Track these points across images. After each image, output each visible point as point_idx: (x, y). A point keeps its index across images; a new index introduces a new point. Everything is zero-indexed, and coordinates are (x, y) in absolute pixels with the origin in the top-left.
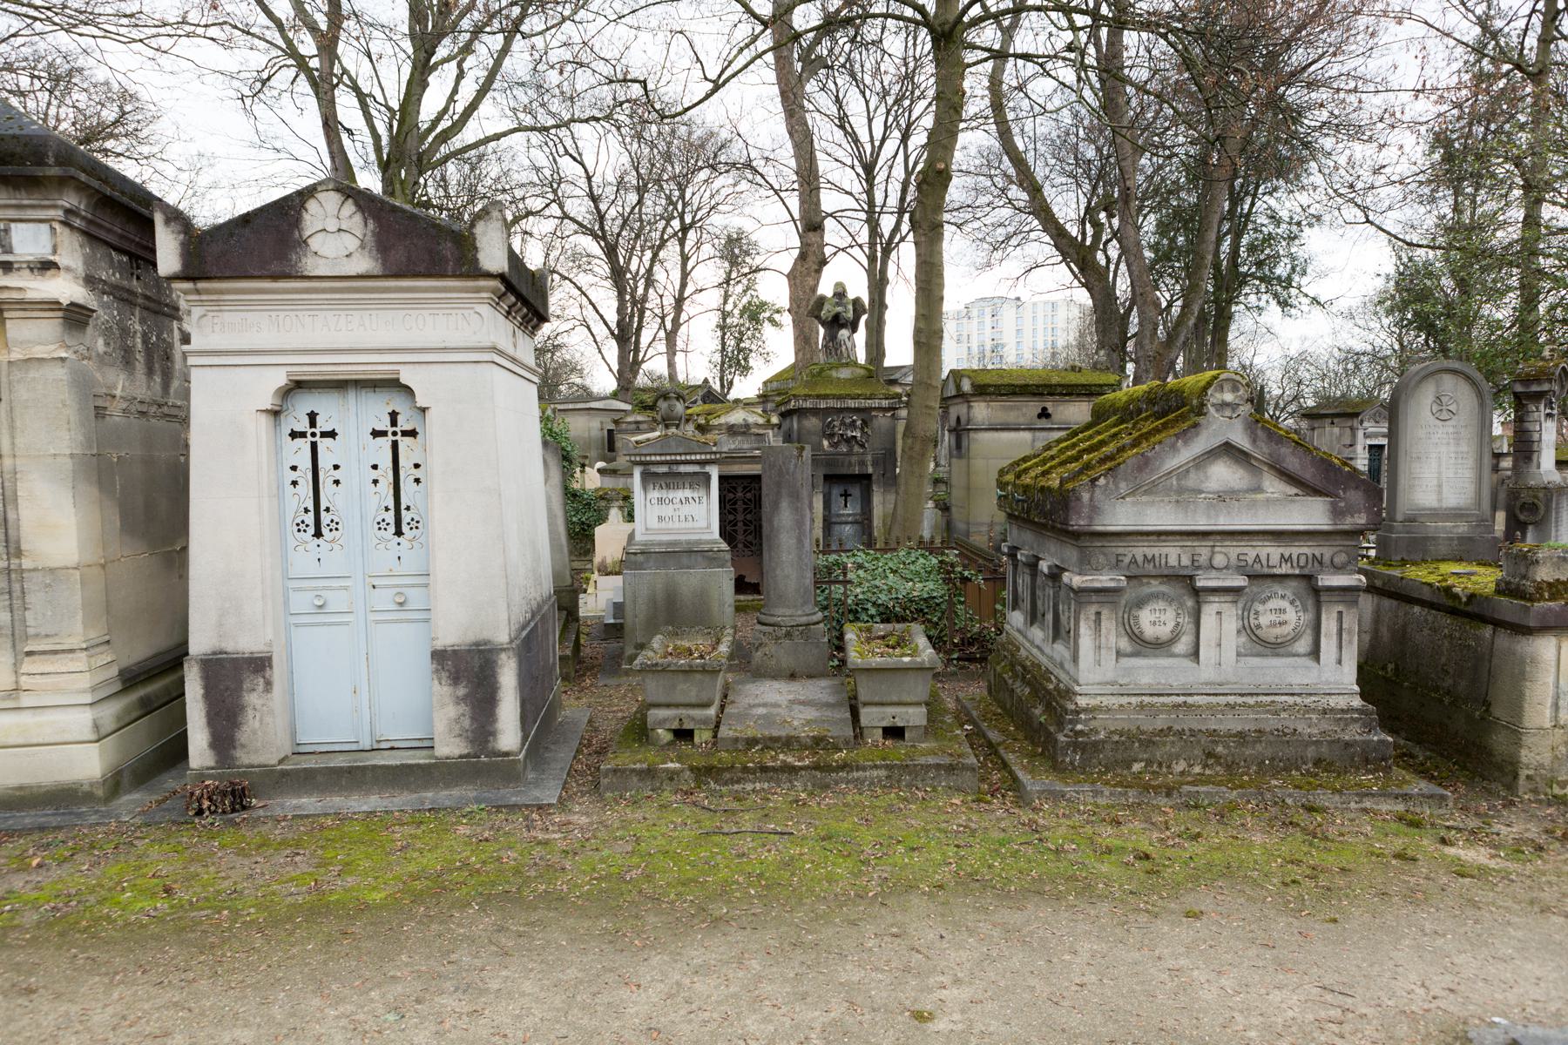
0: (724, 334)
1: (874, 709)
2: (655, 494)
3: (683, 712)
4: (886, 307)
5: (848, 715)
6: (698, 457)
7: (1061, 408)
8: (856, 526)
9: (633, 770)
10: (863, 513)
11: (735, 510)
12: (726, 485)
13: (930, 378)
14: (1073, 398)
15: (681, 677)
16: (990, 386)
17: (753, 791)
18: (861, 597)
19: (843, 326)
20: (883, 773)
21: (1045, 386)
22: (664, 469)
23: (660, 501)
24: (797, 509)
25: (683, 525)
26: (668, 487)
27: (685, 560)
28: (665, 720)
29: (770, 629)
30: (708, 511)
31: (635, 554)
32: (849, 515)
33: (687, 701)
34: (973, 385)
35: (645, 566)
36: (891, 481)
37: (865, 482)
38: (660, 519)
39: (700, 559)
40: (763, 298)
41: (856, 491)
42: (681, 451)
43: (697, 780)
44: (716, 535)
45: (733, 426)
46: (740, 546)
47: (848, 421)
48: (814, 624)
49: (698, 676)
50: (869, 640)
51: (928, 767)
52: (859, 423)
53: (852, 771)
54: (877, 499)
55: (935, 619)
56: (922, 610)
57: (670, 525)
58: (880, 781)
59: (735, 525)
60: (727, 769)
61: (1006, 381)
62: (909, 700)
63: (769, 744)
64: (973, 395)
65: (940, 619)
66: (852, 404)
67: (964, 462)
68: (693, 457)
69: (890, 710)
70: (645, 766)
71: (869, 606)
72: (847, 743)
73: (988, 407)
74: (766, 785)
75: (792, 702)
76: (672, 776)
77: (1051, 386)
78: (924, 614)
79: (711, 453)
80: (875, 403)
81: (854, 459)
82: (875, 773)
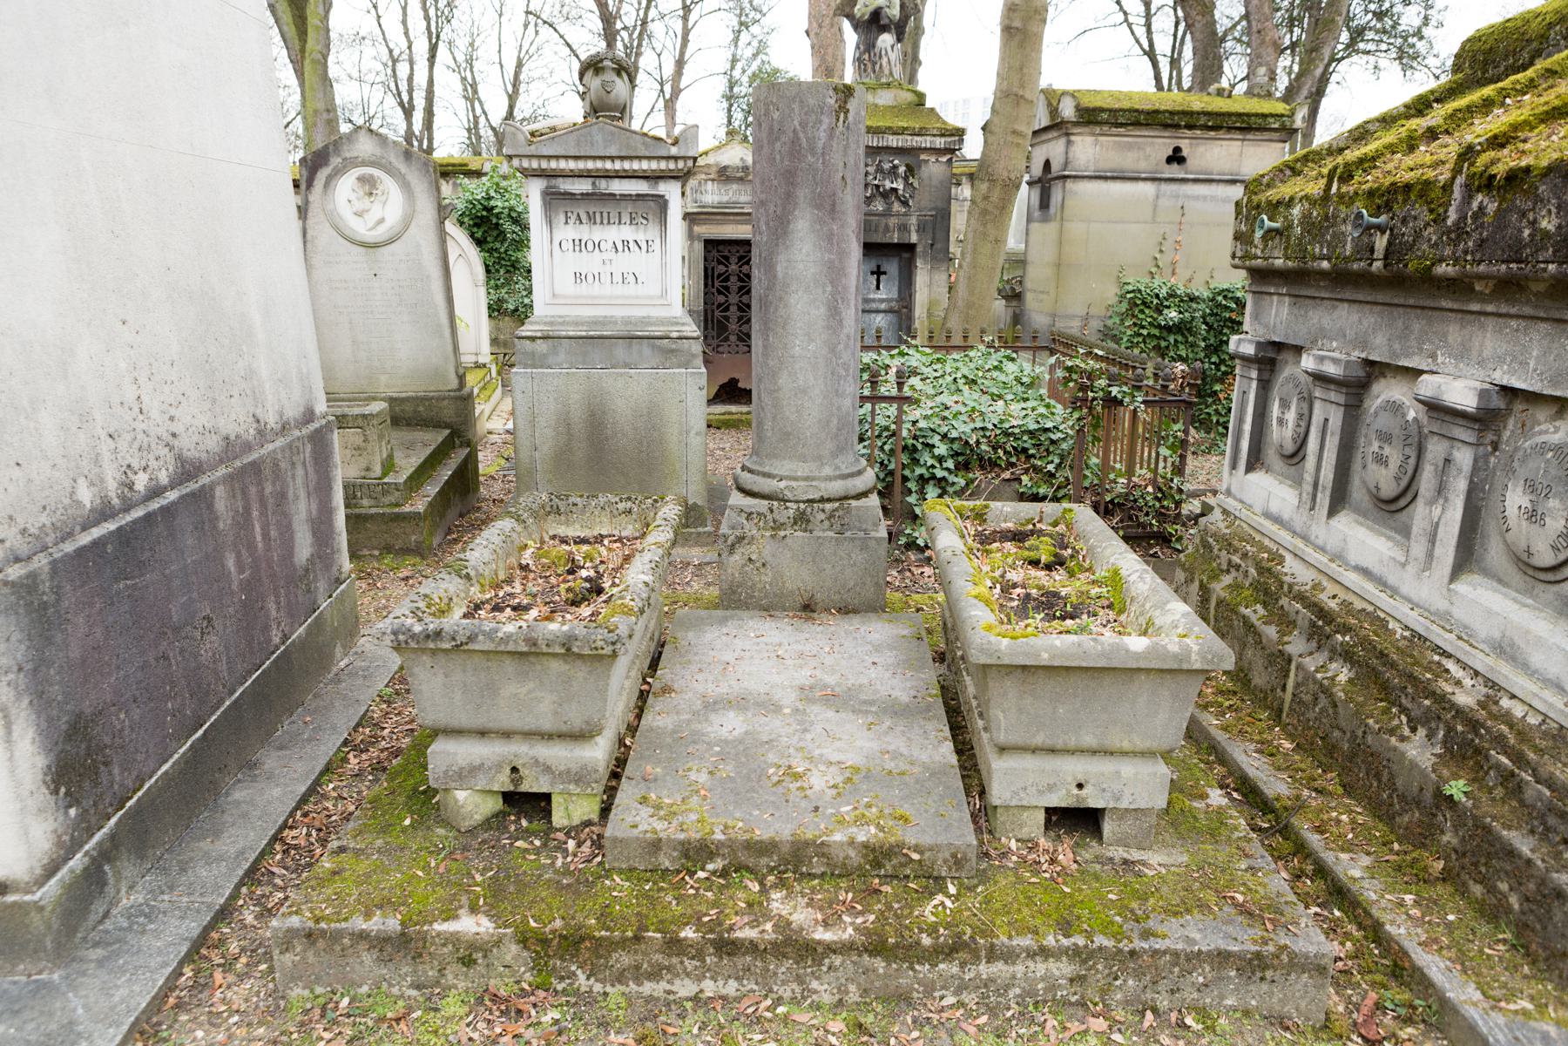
0: (731, 105)
1: (1029, 762)
2: (568, 232)
3: (521, 751)
4: (920, 64)
5: (948, 749)
6: (645, 165)
7: (1201, 149)
8: (890, 317)
9: (362, 936)
10: (901, 298)
11: (727, 288)
12: (714, 253)
13: (1022, 86)
14: (1221, 134)
15: (509, 665)
16: (1102, 110)
17: (695, 999)
18: (922, 424)
19: (884, 29)
20: (1063, 969)
21: (1184, 113)
22: (583, 186)
23: (579, 245)
24: (830, 237)
25: (619, 290)
26: (591, 219)
27: (620, 350)
28: (474, 770)
29: (762, 505)
30: (664, 265)
31: (533, 339)
32: (882, 301)
33: (530, 723)
34: (1078, 108)
35: (551, 360)
36: (941, 255)
37: (906, 255)
38: (578, 277)
40: (776, 63)
41: (892, 267)
42: (613, 151)
43: (538, 966)
44: (677, 310)
45: (725, 168)
46: (733, 338)
47: (887, 166)
48: (858, 496)
49: (556, 666)
50: (984, 539)
51: (1194, 959)
52: (902, 169)
53: (976, 958)
54: (922, 277)
55: (1051, 467)
56: (1025, 450)
57: (596, 289)
58: (1052, 988)
59: (727, 309)
60: (623, 944)
61: (1126, 105)
62: (1126, 745)
63: (743, 857)
64: (1076, 124)
65: (1058, 467)
66: (893, 141)
67: (1051, 228)
68: (636, 165)
69: (1074, 768)
70: (393, 924)
71: (936, 440)
72: (958, 862)
74: (731, 988)
75: (809, 694)
76: (469, 954)
77: (1191, 114)
78: (1029, 457)
79: (668, 158)
80: (926, 142)
81: (893, 221)
82: (1040, 968)
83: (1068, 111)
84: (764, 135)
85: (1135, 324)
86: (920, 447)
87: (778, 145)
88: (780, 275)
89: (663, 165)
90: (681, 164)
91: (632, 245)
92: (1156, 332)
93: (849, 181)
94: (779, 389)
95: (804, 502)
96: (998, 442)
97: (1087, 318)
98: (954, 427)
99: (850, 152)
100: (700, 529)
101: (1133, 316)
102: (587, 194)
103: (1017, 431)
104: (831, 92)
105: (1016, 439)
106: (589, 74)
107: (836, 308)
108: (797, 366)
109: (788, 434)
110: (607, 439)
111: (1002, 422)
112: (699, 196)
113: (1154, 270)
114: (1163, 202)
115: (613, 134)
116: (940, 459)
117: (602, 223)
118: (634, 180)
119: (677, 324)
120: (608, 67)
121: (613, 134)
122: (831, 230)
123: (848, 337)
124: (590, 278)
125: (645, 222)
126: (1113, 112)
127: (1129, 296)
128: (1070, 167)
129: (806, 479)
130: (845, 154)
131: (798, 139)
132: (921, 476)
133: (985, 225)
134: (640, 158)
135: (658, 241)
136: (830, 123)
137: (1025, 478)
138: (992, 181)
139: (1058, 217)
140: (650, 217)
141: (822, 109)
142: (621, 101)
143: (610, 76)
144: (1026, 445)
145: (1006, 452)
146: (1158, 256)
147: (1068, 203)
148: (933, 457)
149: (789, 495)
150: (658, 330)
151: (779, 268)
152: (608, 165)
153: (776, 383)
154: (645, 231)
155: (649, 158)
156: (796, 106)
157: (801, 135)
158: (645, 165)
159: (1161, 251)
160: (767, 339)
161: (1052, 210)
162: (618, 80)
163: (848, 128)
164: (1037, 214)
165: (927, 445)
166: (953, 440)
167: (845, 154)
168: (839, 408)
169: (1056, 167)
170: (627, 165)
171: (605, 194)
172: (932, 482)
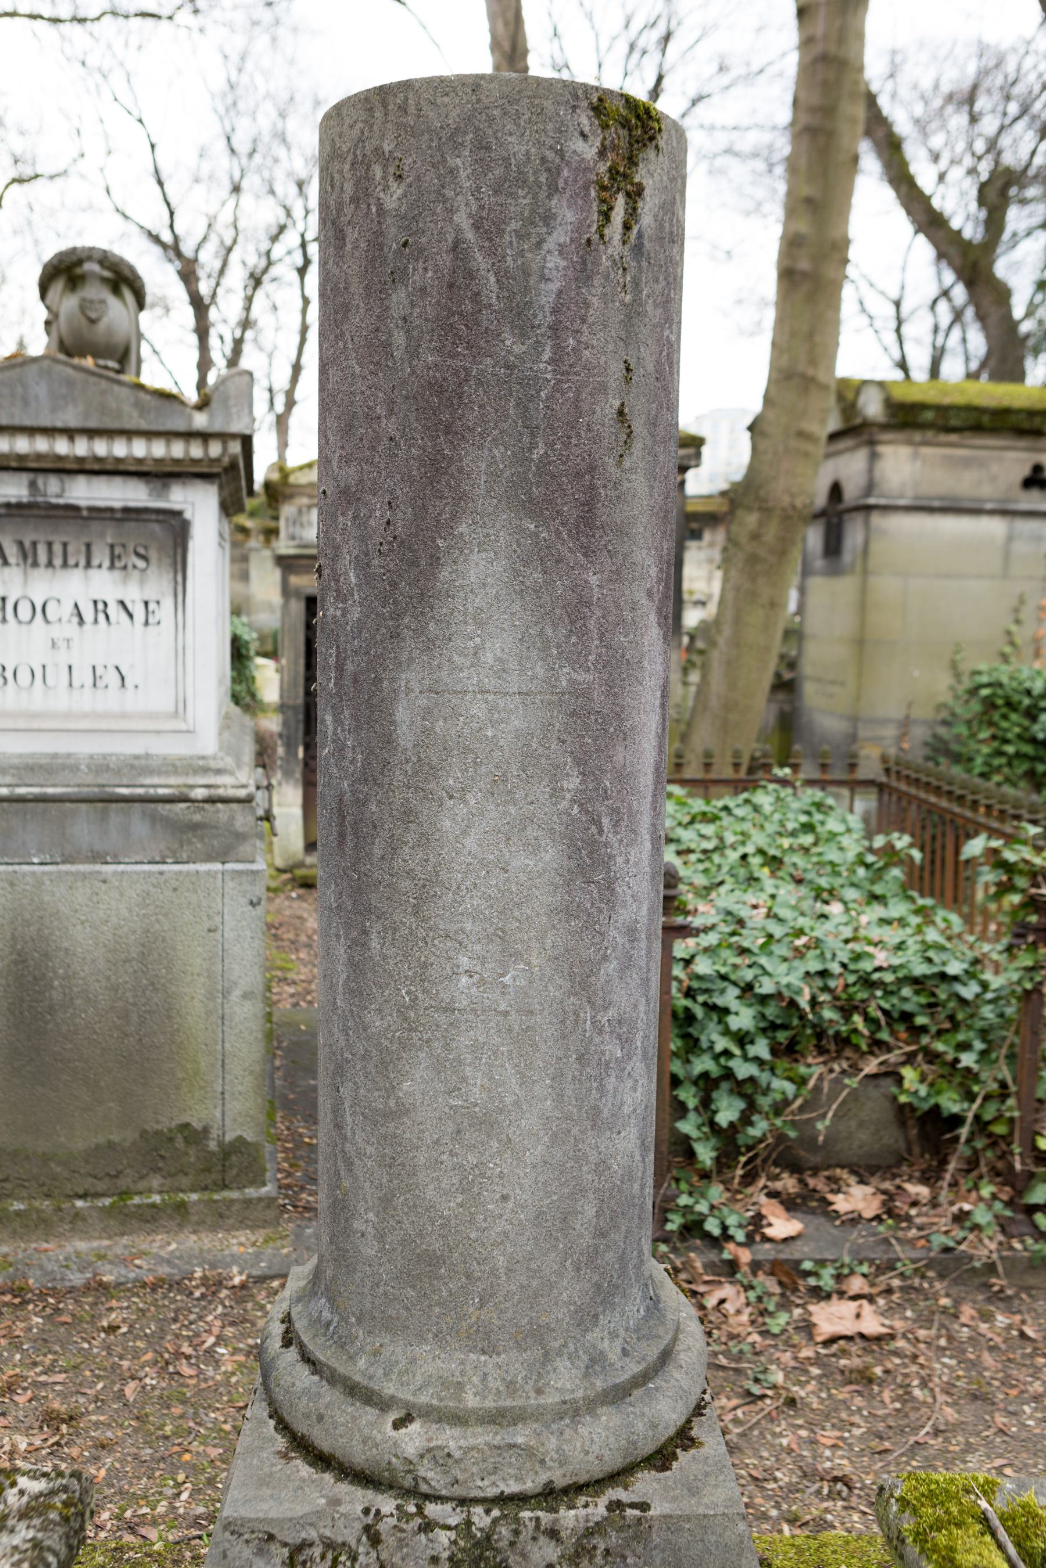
6: (139, 449)
13: (813, 362)
16: (922, 407)
18: (703, 966)
25: (86, 700)
30: (180, 653)
39: (140, 827)
42: (70, 418)
56: (906, 1017)
57: (37, 699)
64: (886, 427)
67: (845, 586)
68: (120, 449)
71: (730, 998)
73: (915, 456)
79: (189, 435)
83: (872, 407)
84: (353, 267)
85: (994, 737)
86: (699, 1012)
87: (399, 298)
88: (405, 736)
89: (178, 450)
90: (215, 449)
91: (113, 610)
92: (1028, 749)
93: (639, 426)
94: (402, 1111)
95: (489, 1503)
96: (850, 998)
97: (906, 724)
98: (766, 973)
99: (644, 332)
100: (251, 1192)
101: (991, 724)
102: (19, 506)
103: (889, 978)
104: (585, 119)
105: (888, 993)
106: (58, 287)
107: (594, 846)
108: (464, 1041)
109: (433, 1260)
110: (51, 1010)
111: (857, 957)
112: (298, 531)
113: (1008, 649)
114: (1019, 547)
115: (70, 383)
116: (742, 1039)
117: (50, 564)
118: (118, 481)
119: (206, 770)
120: (93, 274)
121: (70, 383)
122: (579, 588)
123: (632, 933)
124: (24, 676)
125: (141, 564)
126: (942, 410)
127: (985, 692)
128: (876, 492)
129: (496, 1418)
130: (628, 339)
131: (471, 275)
132: (705, 1075)
133: (753, 579)
134: (129, 434)
135: (168, 603)
136: (580, 227)
137: (909, 1074)
138: (766, 510)
139: (858, 568)
140: (153, 554)
141: (554, 173)
142: (119, 338)
143: (94, 291)
144: (908, 1007)
145: (867, 1019)
146: (1013, 628)
147: (875, 547)
148: (727, 1032)
149: (433, 1477)
150: (163, 785)
151: (401, 714)
152: (62, 447)
153: (391, 1090)
154: (142, 582)
155: (149, 435)
156: (462, 163)
157: (480, 261)
158: (139, 449)
159: (1018, 622)
160: (359, 943)
161: (847, 557)
162: (112, 301)
163: (638, 249)
164: (819, 563)
165: (714, 1008)
166: (764, 999)
167: (628, 339)
168: (602, 1167)
169: (851, 493)
170: (100, 447)
171: (57, 507)
172: (725, 1085)
